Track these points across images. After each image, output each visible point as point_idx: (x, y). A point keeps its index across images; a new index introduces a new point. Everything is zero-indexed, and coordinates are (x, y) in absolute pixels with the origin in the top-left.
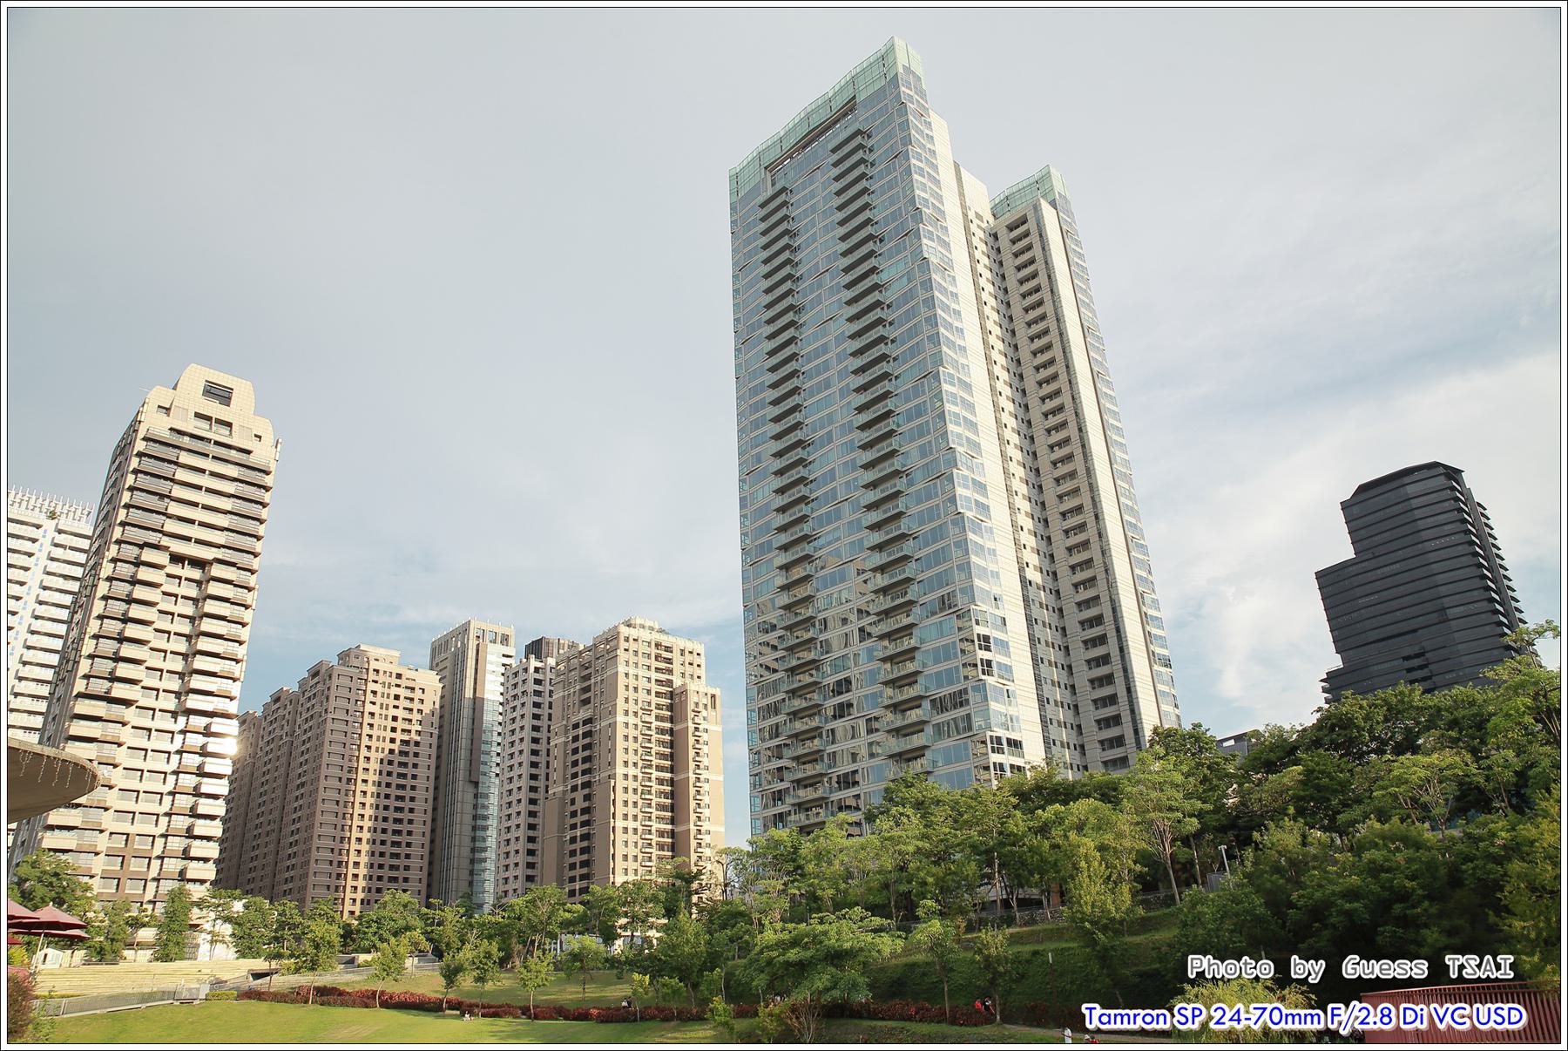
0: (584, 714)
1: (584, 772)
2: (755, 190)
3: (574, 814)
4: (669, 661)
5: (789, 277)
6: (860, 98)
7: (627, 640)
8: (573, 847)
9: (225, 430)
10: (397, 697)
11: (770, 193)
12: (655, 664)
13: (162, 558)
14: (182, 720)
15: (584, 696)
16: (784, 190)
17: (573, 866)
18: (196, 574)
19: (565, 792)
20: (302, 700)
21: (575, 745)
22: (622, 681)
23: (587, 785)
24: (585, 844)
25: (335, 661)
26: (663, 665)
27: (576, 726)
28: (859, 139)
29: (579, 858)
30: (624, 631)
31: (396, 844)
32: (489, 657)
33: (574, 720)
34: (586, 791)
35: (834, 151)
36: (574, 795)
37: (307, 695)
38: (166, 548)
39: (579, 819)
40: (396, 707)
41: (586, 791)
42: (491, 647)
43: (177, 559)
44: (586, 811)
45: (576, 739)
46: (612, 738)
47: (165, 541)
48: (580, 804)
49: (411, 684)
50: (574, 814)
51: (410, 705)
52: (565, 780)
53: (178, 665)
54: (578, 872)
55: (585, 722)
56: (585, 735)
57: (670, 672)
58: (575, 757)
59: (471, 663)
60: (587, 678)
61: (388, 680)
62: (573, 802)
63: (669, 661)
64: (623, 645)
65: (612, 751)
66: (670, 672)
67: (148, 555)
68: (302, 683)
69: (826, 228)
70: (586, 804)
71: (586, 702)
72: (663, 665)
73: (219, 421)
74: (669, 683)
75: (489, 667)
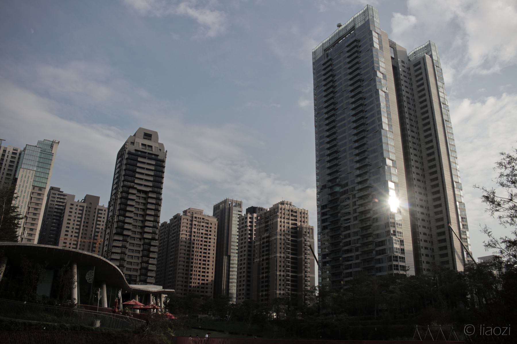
0: (266, 235)
1: (266, 255)
2: (321, 58)
3: (263, 269)
4: (296, 216)
5: (357, 52)
6: (357, 26)
7: (281, 209)
8: (263, 280)
9: (150, 149)
10: (203, 226)
11: (326, 60)
12: (291, 218)
13: (135, 192)
14: (142, 241)
15: (266, 228)
16: (330, 60)
17: (262, 287)
18: (144, 196)
19: (260, 261)
20: (171, 226)
21: (263, 245)
22: (279, 224)
23: (267, 259)
24: (267, 279)
25: (182, 214)
26: (293, 218)
27: (264, 239)
28: (355, 44)
29: (265, 284)
30: (280, 206)
31: (204, 272)
32: (234, 212)
33: (263, 236)
34: (267, 261)
35: (347, 46)
36: (263, 262)
37: (173, 225)
38: (136, 188)
39: (265, 271)
40: (202, 229)
41: (267, 261)
42: (234, 208)
43: (139, 191)
44: (267, 268)
45: (263, 243)
46: (276, 243)
47: (135, 186)
48: (265, 266)
49: (207, 222)
50: (263, 269)
51: (207, 229)
52: (260, 257)
53: (140, 224)
54: (264, 289)
55: (267, 237)
56: (267, 242)
57: (296, 220)
58: (263, 249)
59: (227, 214)
60: (268, 222)
61: (200, 220)
62: (263, 265)
63: (296, 216)
64: (280, 211)
65: (276, 248)
66: (296, 220)
67: (131, 191)
68: (171, 220)
69: (344, 72)
70: (267, 266)
71: (267, 230)
72: (293, 218)
73: (149, 146)
74: (296, 224)
75: (233, 222)
